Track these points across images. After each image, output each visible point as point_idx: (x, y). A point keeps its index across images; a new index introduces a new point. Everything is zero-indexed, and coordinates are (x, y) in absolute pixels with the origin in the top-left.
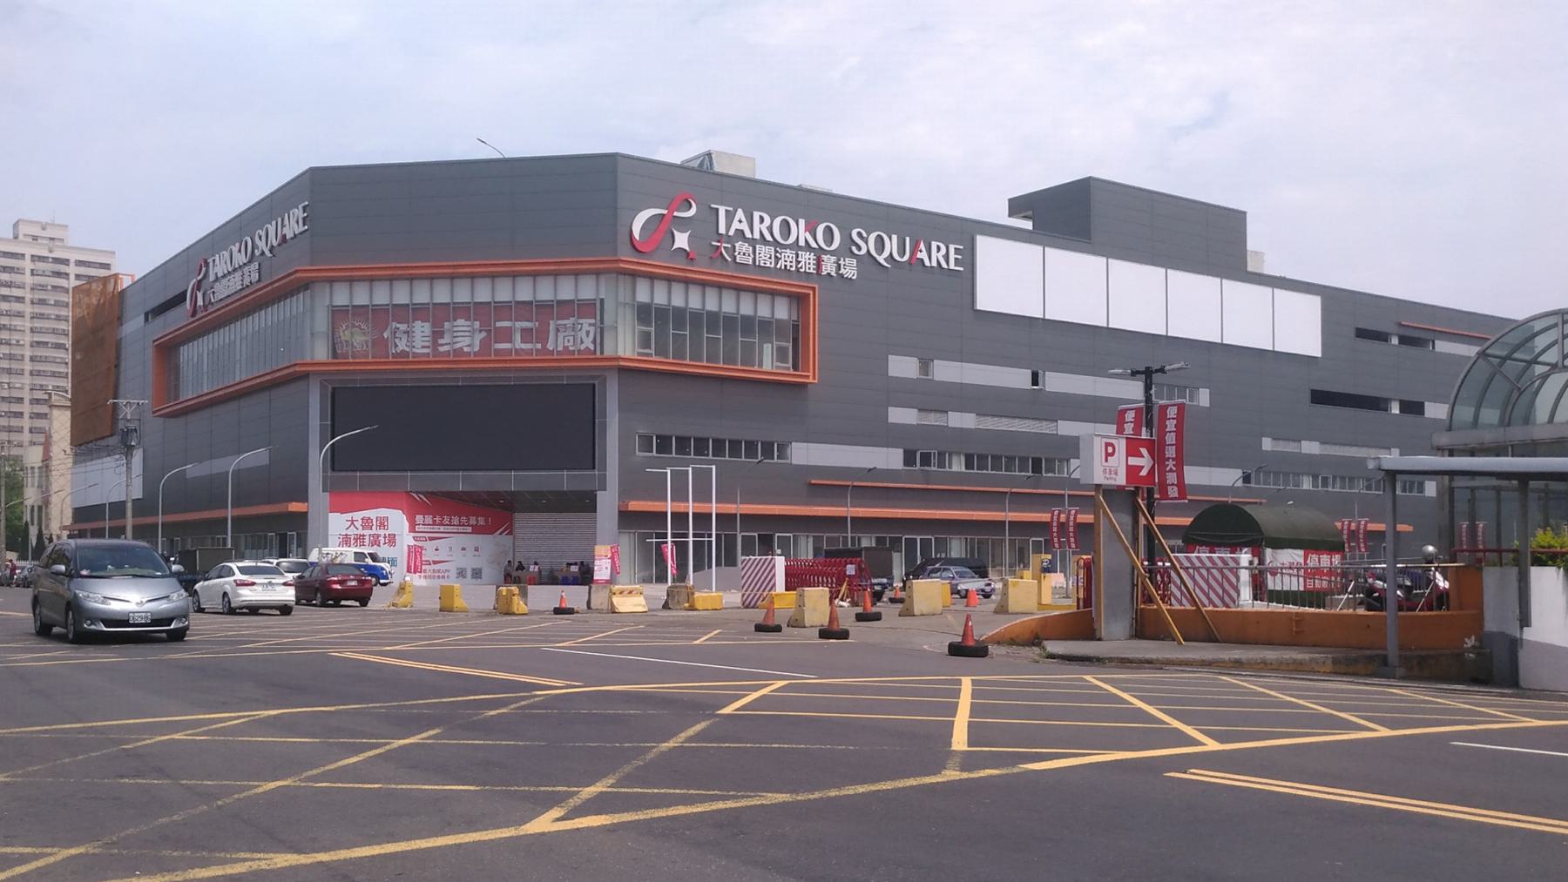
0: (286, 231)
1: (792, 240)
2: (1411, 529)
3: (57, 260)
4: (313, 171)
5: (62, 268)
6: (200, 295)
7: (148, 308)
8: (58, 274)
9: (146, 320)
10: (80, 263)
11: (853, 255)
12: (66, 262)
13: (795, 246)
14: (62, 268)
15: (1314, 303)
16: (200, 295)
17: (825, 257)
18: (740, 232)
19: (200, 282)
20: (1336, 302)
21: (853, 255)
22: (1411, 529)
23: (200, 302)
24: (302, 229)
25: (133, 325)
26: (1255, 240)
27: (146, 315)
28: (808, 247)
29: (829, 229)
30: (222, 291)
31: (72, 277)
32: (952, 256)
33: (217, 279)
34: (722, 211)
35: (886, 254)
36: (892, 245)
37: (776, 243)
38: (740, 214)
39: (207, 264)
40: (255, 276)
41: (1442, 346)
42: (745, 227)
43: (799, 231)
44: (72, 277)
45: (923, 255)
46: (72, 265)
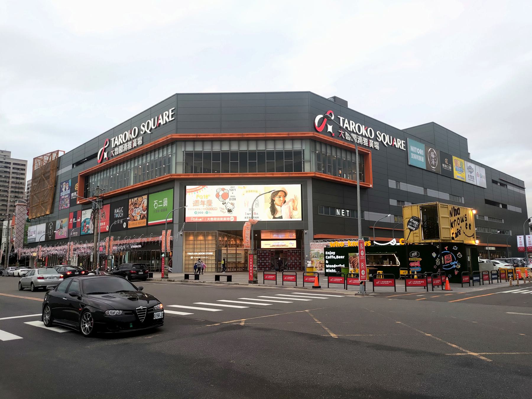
0: (160, 121)
1: (361, 133)
2: (510, 246)
3: (6, 163)
4: (178, 96)
5: (8, 165)
6: (105, 154)
7: (74, 163)
8: (6, 167)
9: (73, 167)
10: (14, 164)
11: (377, 141)
12: (10, 163)
13: (362, 135)
14: (8, 165)
15: (483, 172)
16: (105, 154)
17: (370, 141)
18: (346, 128)
19: (105, 149)
20: (489, 171)
21: (377, 141)
22: (510, 246)
23: (105, 156)
24: (171, 119)
25: (65, 170)
26: (471, 149)
27: (73, 165)
28: (365, 136)
29: (370, 130)
30: (119, 150)
31: (11, 168)
32: (403, 145)
33: (116, 146)
34: (341, 118)
35: (386, 142)
36: (387, 138)
37: (356, 133)
38: (346, 121)
39: (110, 141)
40: (140, 142)
41: (510, 187)
42: (348, 126)
43: (363, 128)
44: (11, 168)
45: (395, 143)
46: (12, 164)
